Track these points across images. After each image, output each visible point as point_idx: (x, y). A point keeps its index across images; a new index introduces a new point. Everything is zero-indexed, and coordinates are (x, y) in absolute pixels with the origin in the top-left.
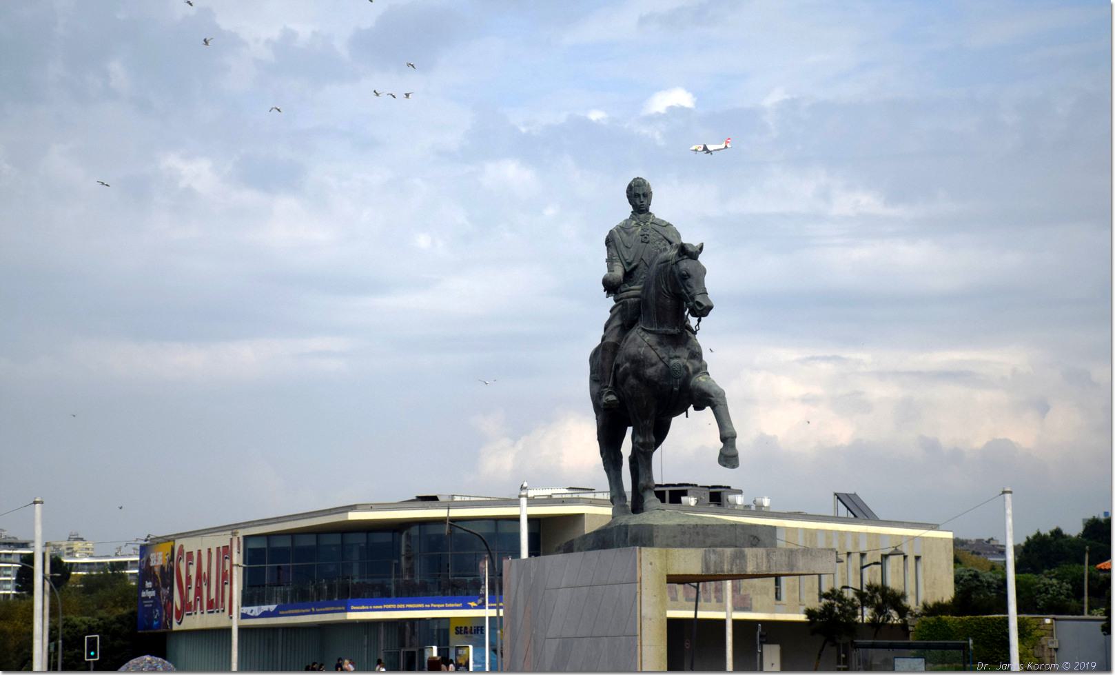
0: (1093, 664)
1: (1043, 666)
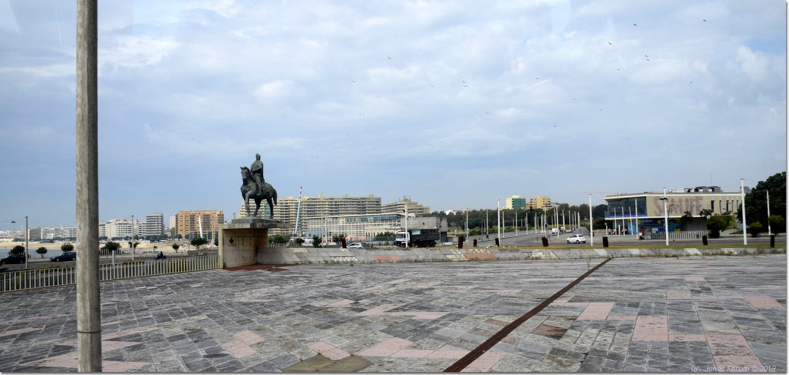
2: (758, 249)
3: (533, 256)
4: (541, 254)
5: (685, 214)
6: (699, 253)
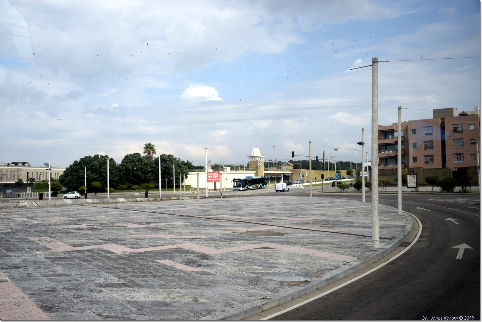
0: (473, 317)
1: (451, 318)
2: (154, 199)
3: (20, 205)
4: (26, 204)
5: (18, 181)
6: (125, 201)
